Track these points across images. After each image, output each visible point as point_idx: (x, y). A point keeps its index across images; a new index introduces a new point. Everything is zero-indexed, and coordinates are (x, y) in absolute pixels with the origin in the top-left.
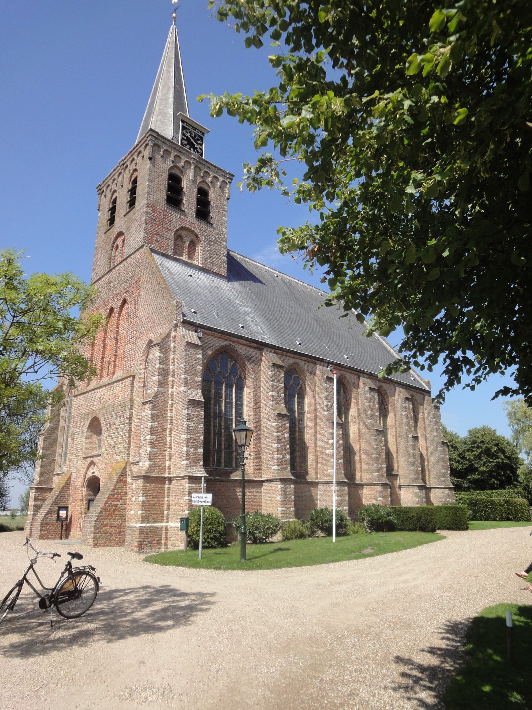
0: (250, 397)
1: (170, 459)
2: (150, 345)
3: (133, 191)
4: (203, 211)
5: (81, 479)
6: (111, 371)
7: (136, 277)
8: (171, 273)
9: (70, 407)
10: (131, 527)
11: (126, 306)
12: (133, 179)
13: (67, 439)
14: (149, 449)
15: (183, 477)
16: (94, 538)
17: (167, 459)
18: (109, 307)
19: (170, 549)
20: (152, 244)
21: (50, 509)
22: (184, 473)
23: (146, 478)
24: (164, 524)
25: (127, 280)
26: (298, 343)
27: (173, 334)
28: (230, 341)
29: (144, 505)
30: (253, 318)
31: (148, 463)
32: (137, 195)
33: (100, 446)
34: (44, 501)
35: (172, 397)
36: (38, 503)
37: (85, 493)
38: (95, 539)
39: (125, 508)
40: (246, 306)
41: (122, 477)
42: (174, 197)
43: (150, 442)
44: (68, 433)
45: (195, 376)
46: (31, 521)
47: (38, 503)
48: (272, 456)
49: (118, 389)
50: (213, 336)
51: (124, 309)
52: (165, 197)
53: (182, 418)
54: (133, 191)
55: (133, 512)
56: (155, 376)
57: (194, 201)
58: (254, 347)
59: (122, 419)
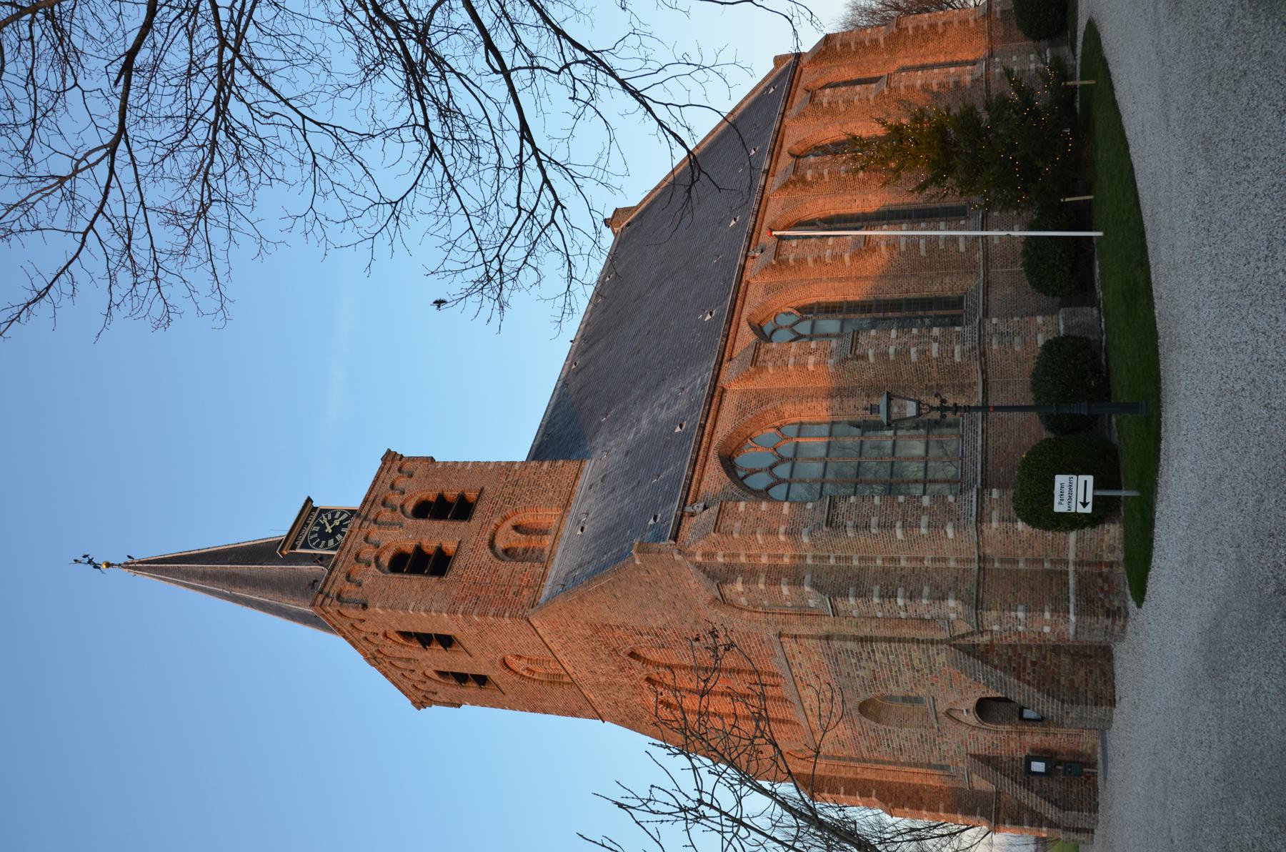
0: (819, 408)
1: (945, 560)
2: (722, 601)
3: (425, 640)
4: (460, 509)
5: (981, 735)
6: (769, 680)
7: (589, 632)
8: (580, 566)
9: (839, 758)
10: (1076, 632)
11: (642, 652)
12: (401, 641)
13: (903, 764)
14: (925, 602)
15: (979, 532)
16: (1096, 704)
17: (943, 565)
18: (646, 685)
19: (1119, 555)
20: (519, 603)
21: (1037, 793)
22: (972, 530)
23: (978, 604)
24: (1071, 568)
25: (594, 650)
26: (709, 317)
27: (699, 558)
28: (708, 448)
29: (1034, 607)
30: (662, 406)
31: (951, 603)
32: (432, 631)
33: (918, 700)
34: (1021, 805)
35: (822, 558)
36: (1026, 817)
37: (1008, 728)
38: (1098, 701)
39: (1039, 647)
40: (639, 420)
41: (982, 654)
42: (431, 563)
43: (911, 598)
44: (890, 763)
45: (780, 514)
46: (1060, 831)
47: (1026, 817)
48: (934, 363)
49: (806, 664)
50: (700, 482)
51: (648, 657)
52: (435, 579)
53: (862, 539)
54: (425, 640)
55: (1047, 629)
56: (781, 592)
57: (438, 525)
58: (720, 403)
59: (865, 655)
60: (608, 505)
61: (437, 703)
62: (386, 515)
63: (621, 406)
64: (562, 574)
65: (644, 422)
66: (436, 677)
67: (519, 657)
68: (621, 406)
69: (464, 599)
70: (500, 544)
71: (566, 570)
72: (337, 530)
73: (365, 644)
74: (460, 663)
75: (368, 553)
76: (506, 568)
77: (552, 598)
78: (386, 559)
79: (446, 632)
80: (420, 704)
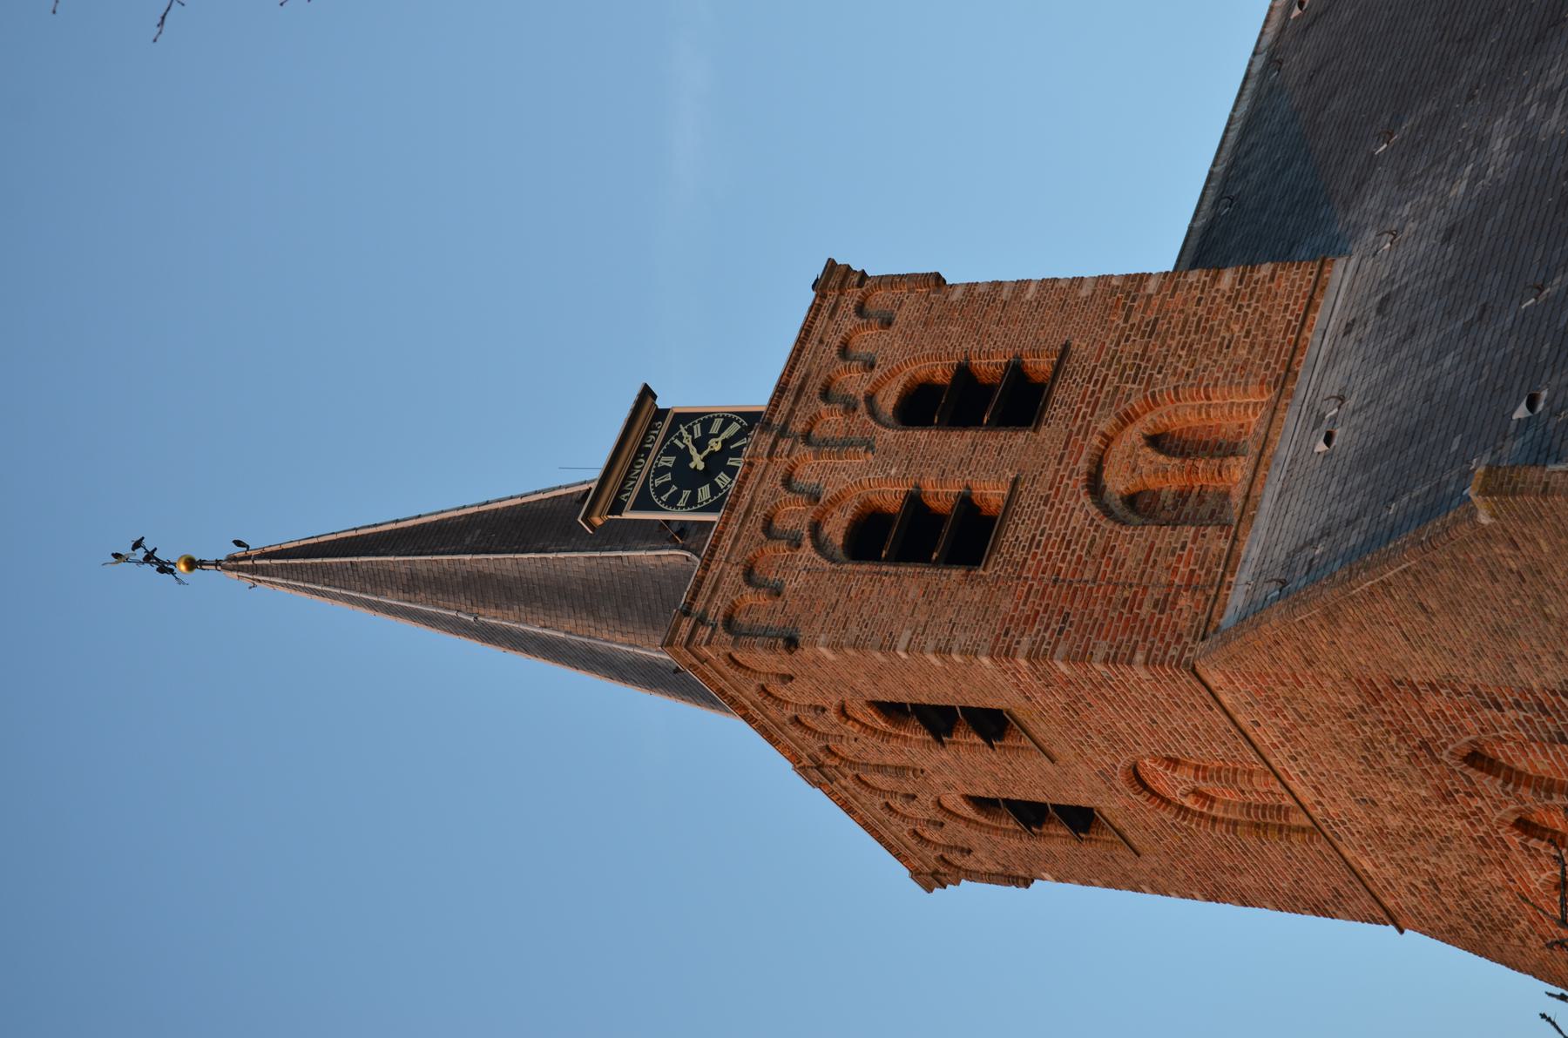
7: (1353, 701)
8: (1326, 533)
20: (1168, 631)
30: (1550, 98)
40: (1482, 142)
60: (1396, 375)
61: (972, 875)
62: (833, 422)
63: (1431, 108)
64: (1279, 554)
65: (1498, 144)
66: (968, 811)
67: (1173, 763)
68: (1431, 108)
69: (1030, 620)
70: (1117, 482)
71: (1289, 543)
72: (716, 463)
73: (796, 733)
74: (1029, 778)
75: (795, 515)
76: (1132, 542)
77: (1254, 613)
78: (836, 528)
79: (992, 703)
80: (932, 877)
